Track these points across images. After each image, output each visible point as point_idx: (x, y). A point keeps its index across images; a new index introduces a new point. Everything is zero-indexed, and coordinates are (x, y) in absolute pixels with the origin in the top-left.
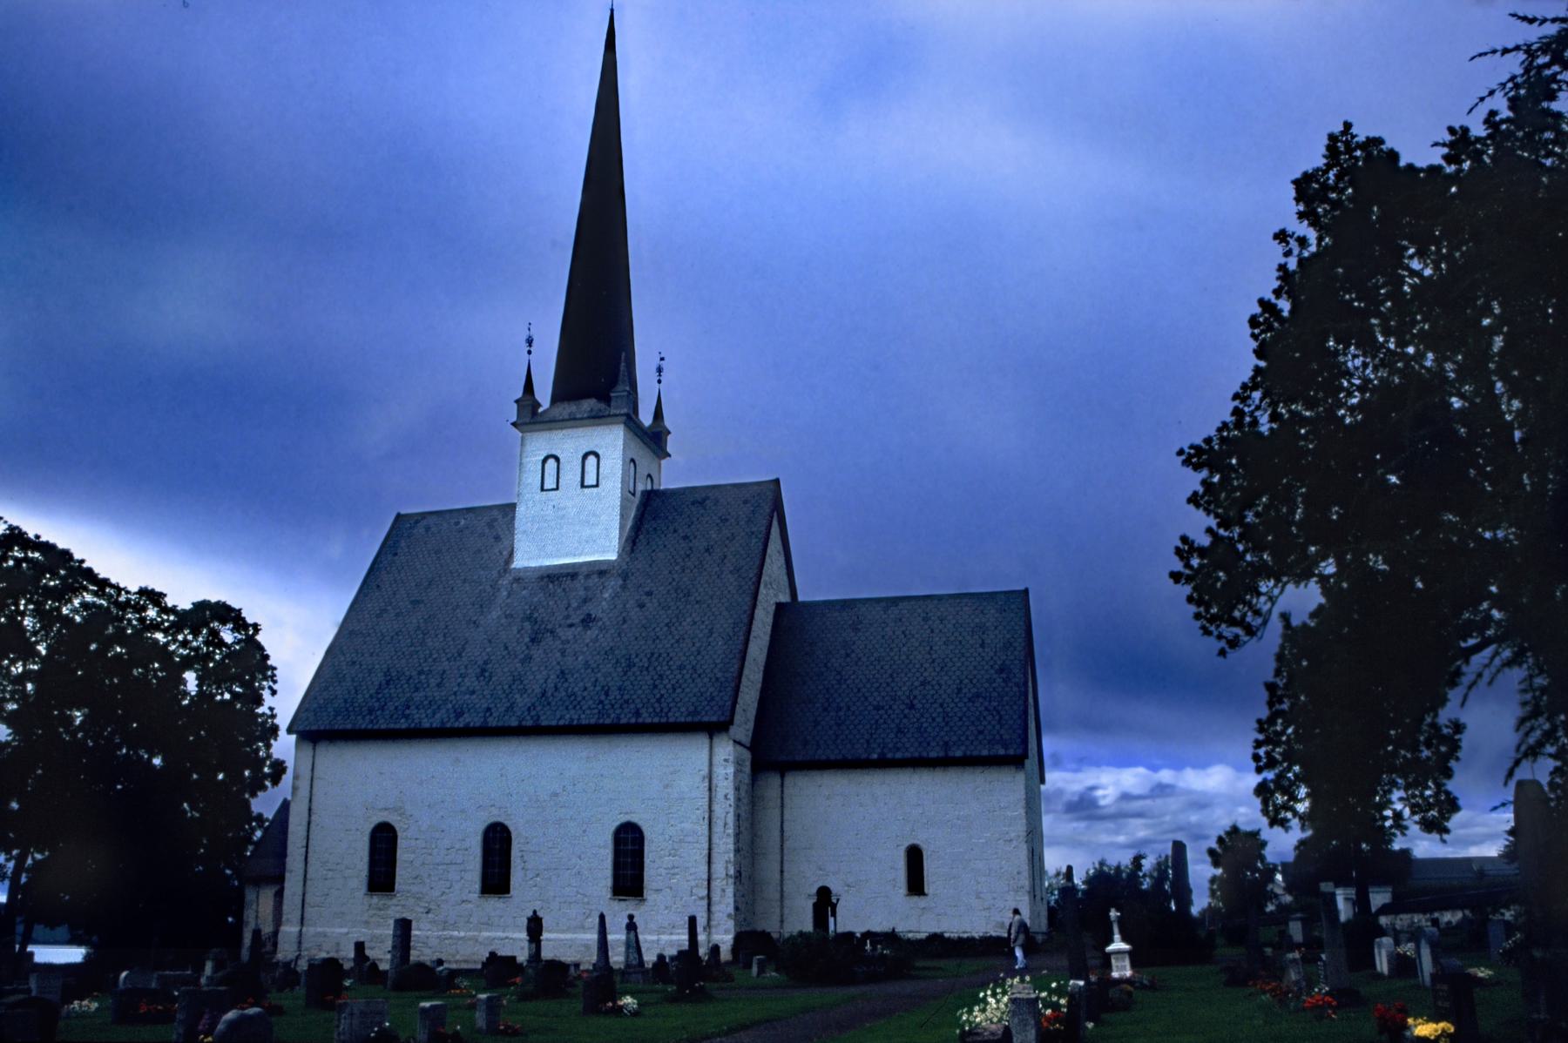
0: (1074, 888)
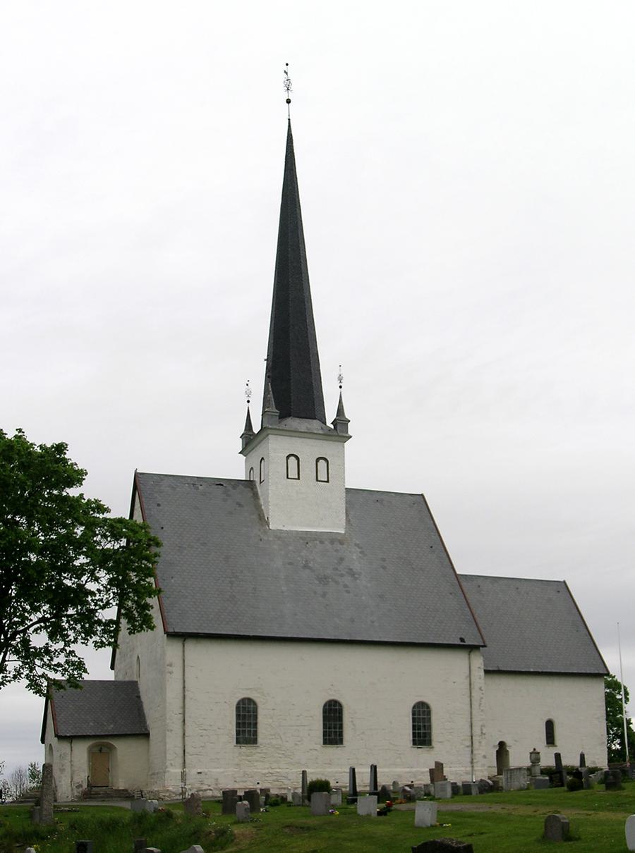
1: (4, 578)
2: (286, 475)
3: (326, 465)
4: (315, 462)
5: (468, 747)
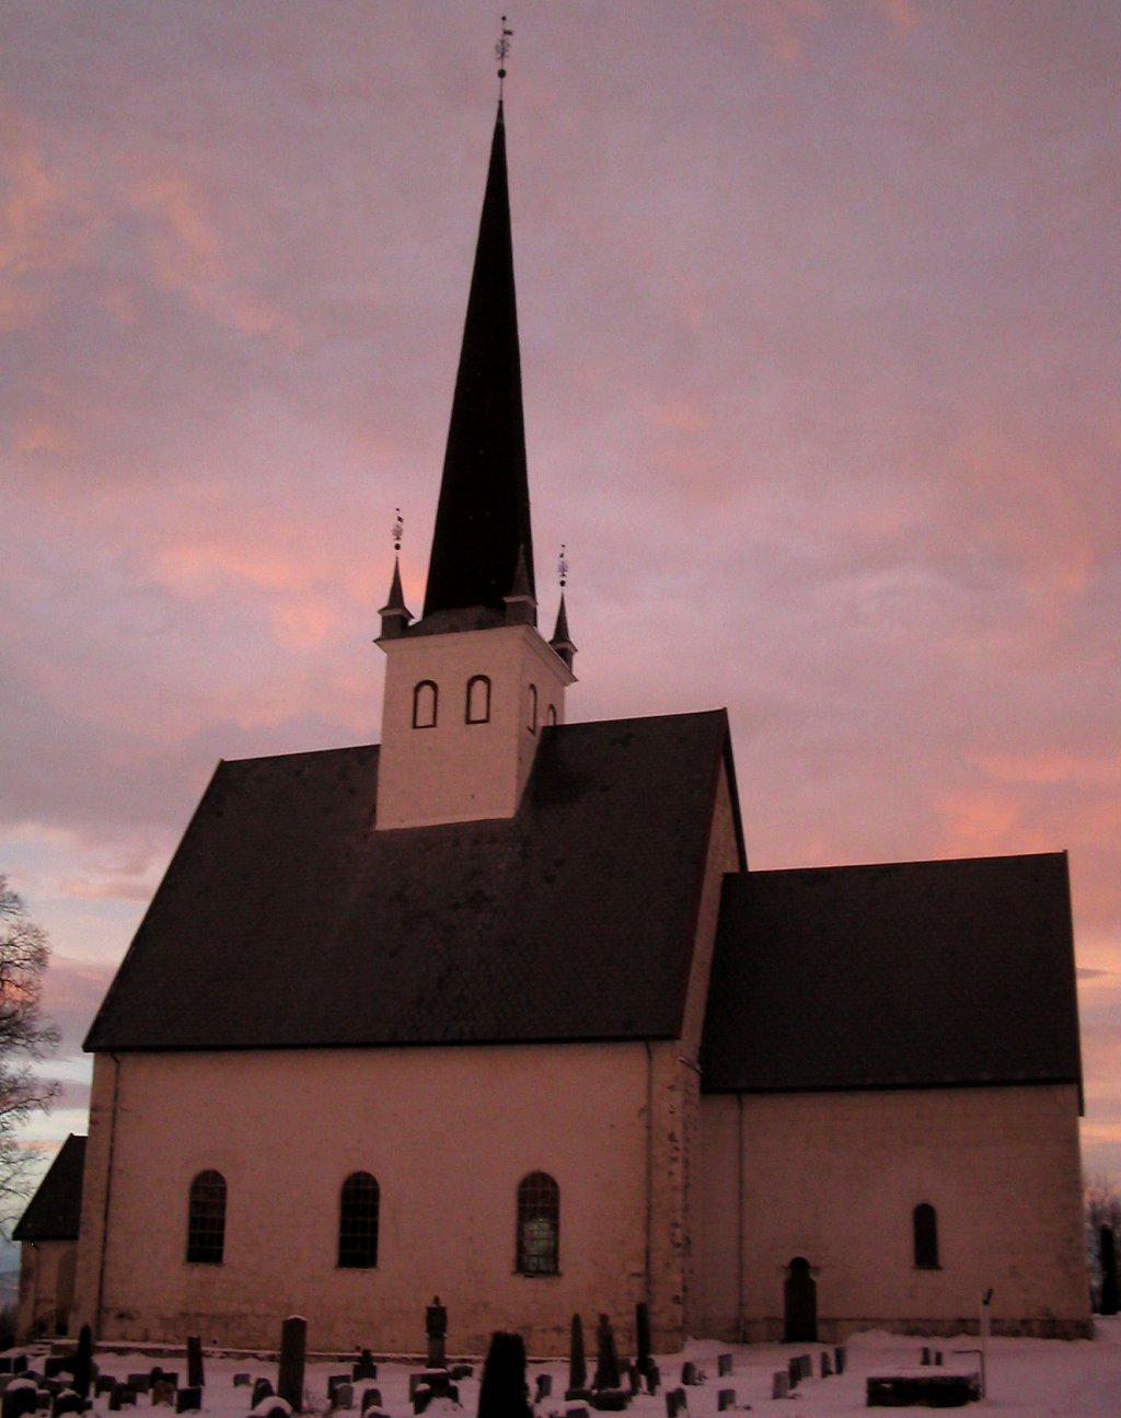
0: (6, 1385)
1: (481, 452)
2: (411, 720)
3: (486, 686)
4: (464, 689)
5: (639, 1275)
